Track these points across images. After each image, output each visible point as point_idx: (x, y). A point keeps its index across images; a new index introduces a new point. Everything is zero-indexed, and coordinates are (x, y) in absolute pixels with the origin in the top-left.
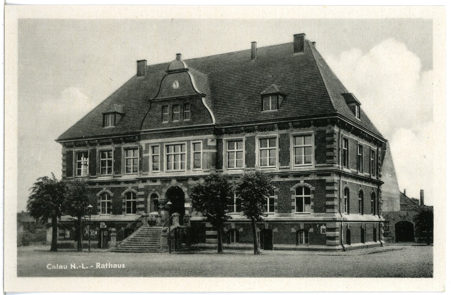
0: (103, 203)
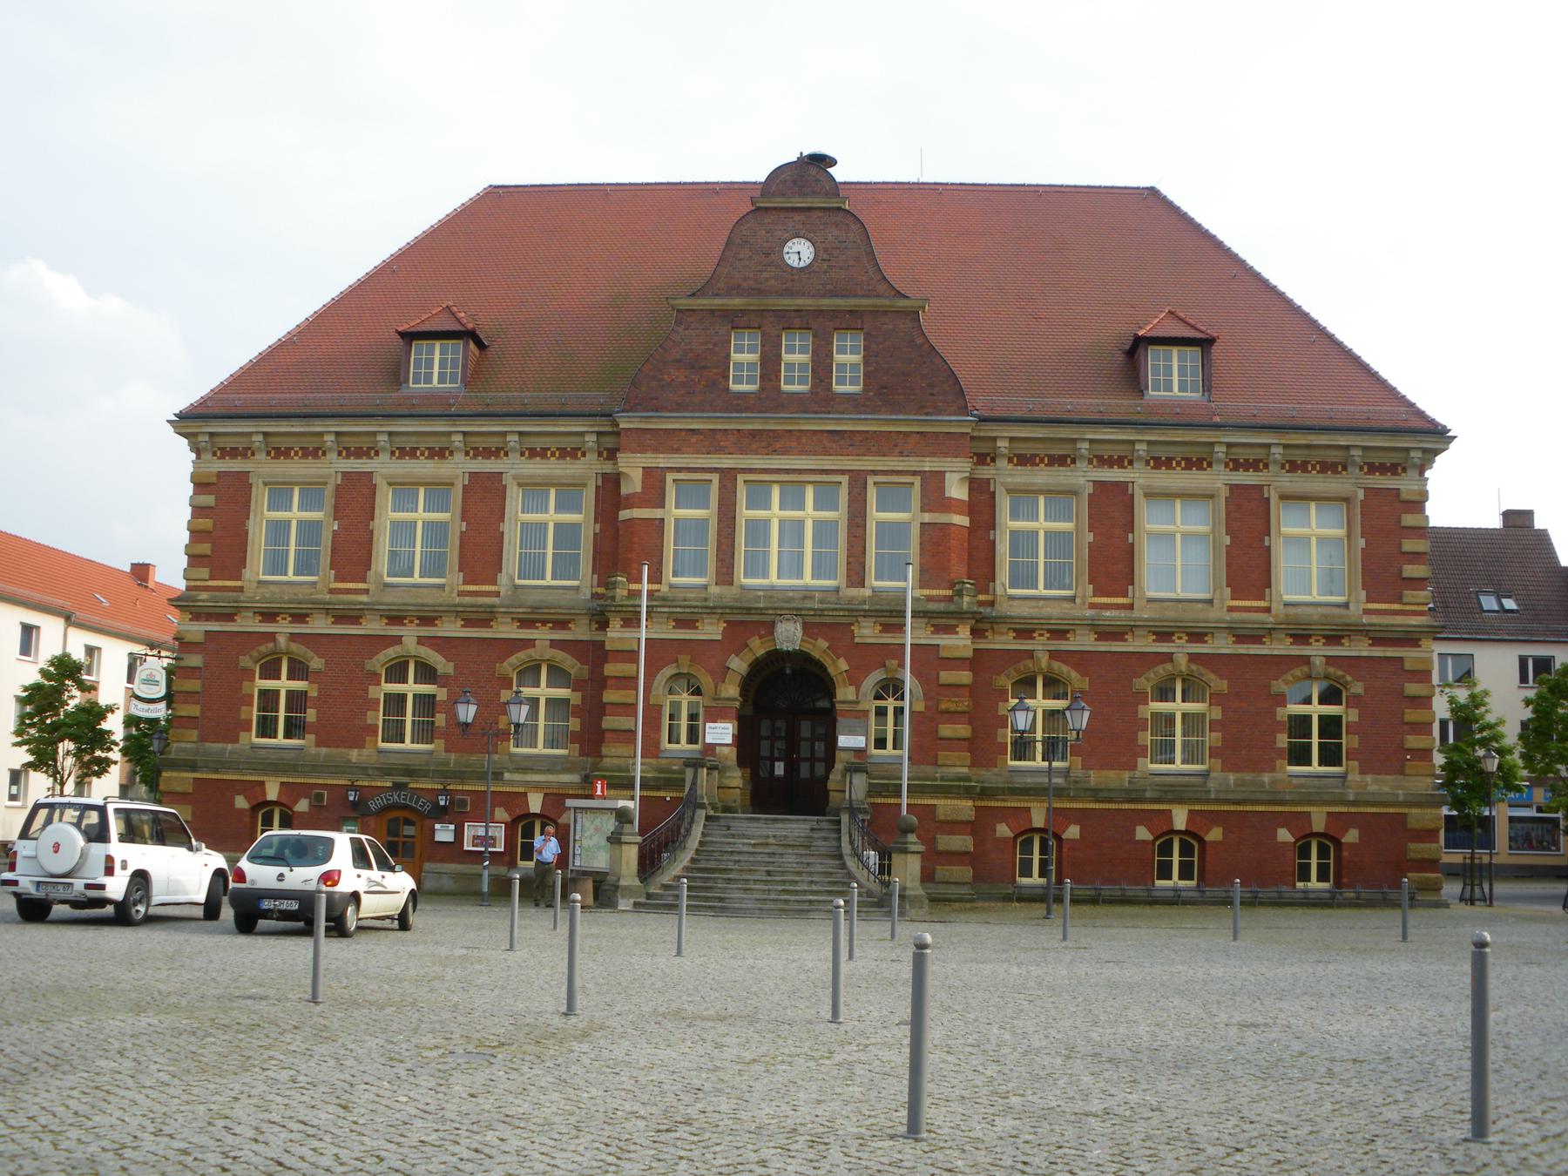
0: (269, 698)
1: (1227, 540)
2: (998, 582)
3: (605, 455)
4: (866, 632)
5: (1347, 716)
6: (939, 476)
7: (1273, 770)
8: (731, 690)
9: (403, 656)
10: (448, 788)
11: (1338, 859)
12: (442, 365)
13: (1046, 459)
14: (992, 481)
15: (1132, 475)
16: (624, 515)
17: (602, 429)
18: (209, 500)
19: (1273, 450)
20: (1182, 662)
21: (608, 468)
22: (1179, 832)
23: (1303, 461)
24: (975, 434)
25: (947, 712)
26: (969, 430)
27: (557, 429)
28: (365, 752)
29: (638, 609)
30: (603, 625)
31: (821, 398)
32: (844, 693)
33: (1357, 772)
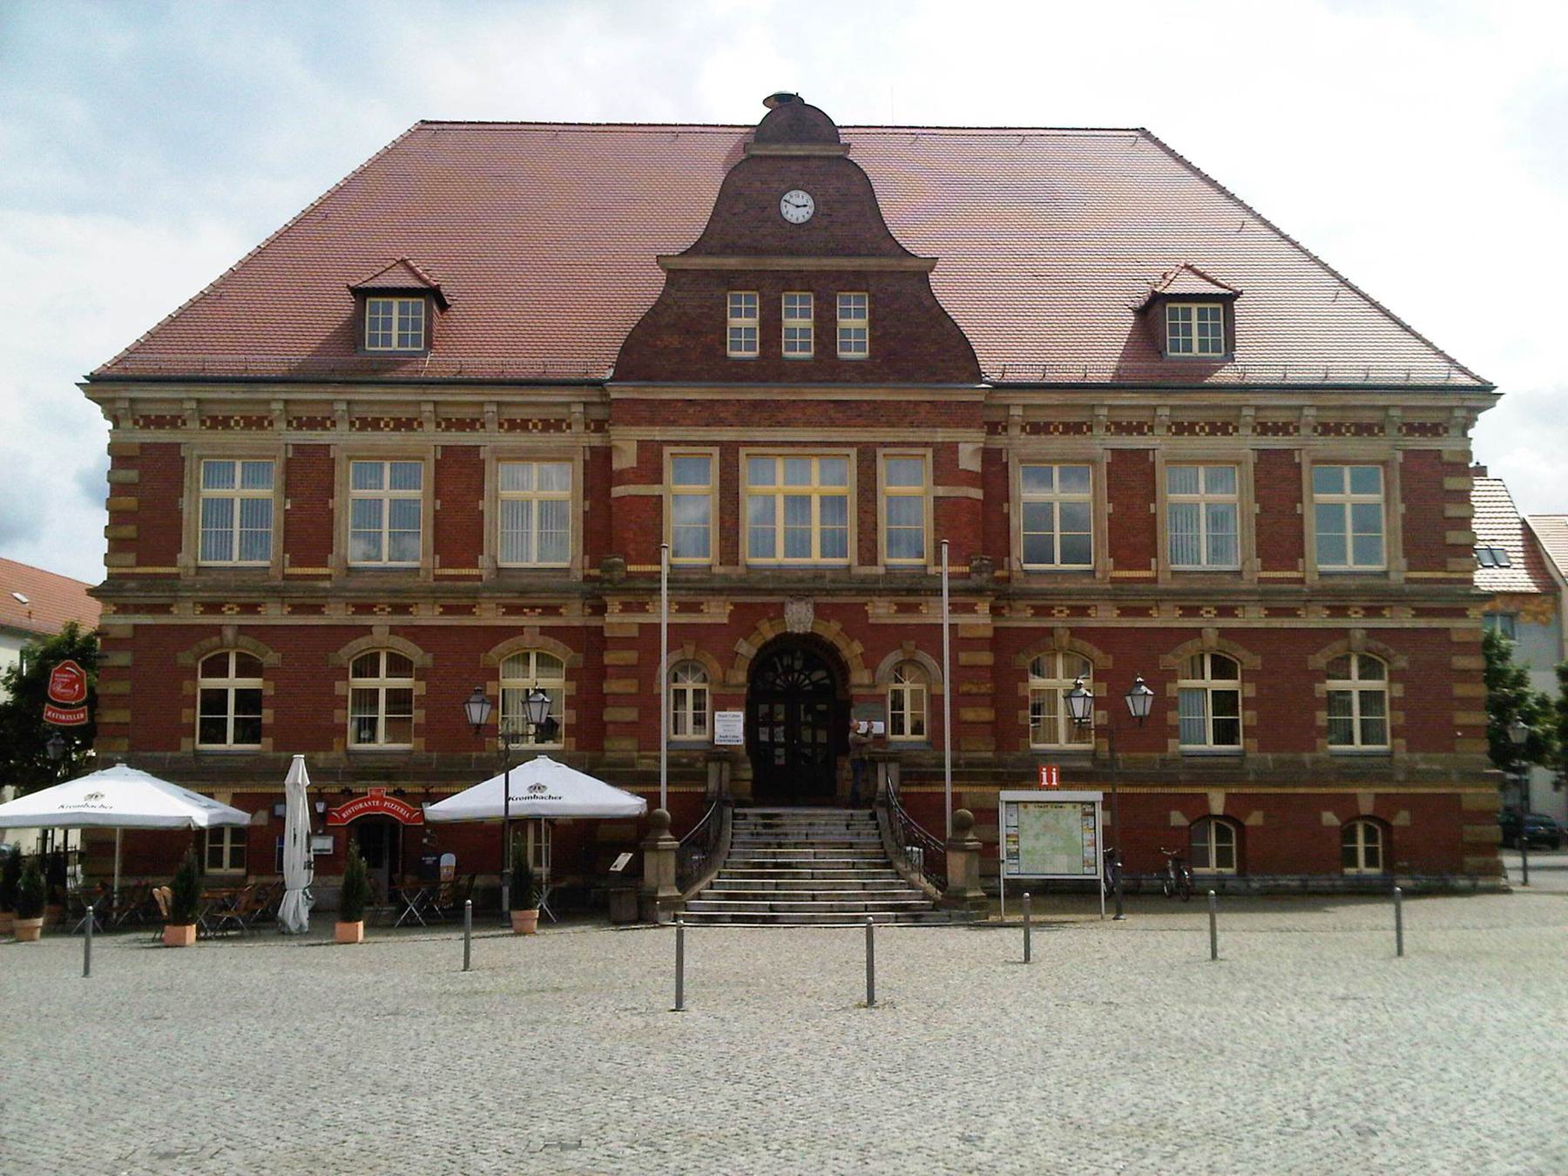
0: (215, 701)
1: (1257, 509)
2: (1013, 557)
3: (592, 427)
4: (881, 611)
5: (1391, 692)
6: (953, 447)
7: (1313, 749)
8: (741, 677)
9: (373, 648)
10: (431, 791)
11: (1388, 843)
12: (403, 325)
13: (1061, 427)
14: (1004, 451)
15: (1153, 442)
16: (618, 491)
17: (589, 399)
18: (132, 475)
19: (1306, 412)
20: (1211, 638)
21: (596, 440)
22: (1217, 817)
23: (1336, 424)
24: (988, 402)
25: (969, 694)
26: (982, 398)
27: (540, 399)
28: (333, 755)
29: (670, 592)
30: (600, 610)
31: (826, 367)
32: (860, 677)
33: (1404, 750)
